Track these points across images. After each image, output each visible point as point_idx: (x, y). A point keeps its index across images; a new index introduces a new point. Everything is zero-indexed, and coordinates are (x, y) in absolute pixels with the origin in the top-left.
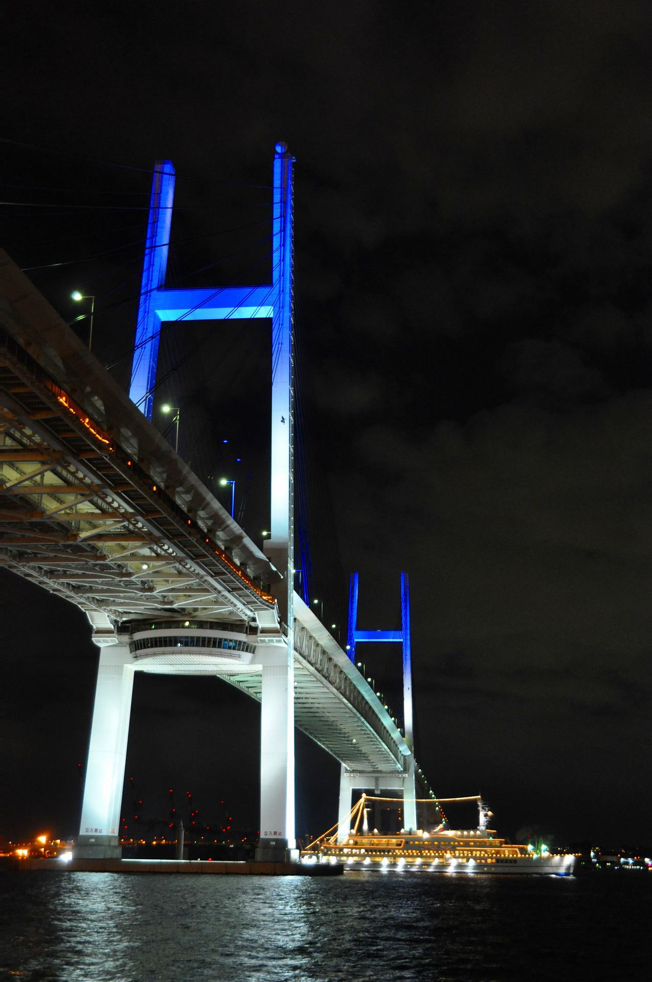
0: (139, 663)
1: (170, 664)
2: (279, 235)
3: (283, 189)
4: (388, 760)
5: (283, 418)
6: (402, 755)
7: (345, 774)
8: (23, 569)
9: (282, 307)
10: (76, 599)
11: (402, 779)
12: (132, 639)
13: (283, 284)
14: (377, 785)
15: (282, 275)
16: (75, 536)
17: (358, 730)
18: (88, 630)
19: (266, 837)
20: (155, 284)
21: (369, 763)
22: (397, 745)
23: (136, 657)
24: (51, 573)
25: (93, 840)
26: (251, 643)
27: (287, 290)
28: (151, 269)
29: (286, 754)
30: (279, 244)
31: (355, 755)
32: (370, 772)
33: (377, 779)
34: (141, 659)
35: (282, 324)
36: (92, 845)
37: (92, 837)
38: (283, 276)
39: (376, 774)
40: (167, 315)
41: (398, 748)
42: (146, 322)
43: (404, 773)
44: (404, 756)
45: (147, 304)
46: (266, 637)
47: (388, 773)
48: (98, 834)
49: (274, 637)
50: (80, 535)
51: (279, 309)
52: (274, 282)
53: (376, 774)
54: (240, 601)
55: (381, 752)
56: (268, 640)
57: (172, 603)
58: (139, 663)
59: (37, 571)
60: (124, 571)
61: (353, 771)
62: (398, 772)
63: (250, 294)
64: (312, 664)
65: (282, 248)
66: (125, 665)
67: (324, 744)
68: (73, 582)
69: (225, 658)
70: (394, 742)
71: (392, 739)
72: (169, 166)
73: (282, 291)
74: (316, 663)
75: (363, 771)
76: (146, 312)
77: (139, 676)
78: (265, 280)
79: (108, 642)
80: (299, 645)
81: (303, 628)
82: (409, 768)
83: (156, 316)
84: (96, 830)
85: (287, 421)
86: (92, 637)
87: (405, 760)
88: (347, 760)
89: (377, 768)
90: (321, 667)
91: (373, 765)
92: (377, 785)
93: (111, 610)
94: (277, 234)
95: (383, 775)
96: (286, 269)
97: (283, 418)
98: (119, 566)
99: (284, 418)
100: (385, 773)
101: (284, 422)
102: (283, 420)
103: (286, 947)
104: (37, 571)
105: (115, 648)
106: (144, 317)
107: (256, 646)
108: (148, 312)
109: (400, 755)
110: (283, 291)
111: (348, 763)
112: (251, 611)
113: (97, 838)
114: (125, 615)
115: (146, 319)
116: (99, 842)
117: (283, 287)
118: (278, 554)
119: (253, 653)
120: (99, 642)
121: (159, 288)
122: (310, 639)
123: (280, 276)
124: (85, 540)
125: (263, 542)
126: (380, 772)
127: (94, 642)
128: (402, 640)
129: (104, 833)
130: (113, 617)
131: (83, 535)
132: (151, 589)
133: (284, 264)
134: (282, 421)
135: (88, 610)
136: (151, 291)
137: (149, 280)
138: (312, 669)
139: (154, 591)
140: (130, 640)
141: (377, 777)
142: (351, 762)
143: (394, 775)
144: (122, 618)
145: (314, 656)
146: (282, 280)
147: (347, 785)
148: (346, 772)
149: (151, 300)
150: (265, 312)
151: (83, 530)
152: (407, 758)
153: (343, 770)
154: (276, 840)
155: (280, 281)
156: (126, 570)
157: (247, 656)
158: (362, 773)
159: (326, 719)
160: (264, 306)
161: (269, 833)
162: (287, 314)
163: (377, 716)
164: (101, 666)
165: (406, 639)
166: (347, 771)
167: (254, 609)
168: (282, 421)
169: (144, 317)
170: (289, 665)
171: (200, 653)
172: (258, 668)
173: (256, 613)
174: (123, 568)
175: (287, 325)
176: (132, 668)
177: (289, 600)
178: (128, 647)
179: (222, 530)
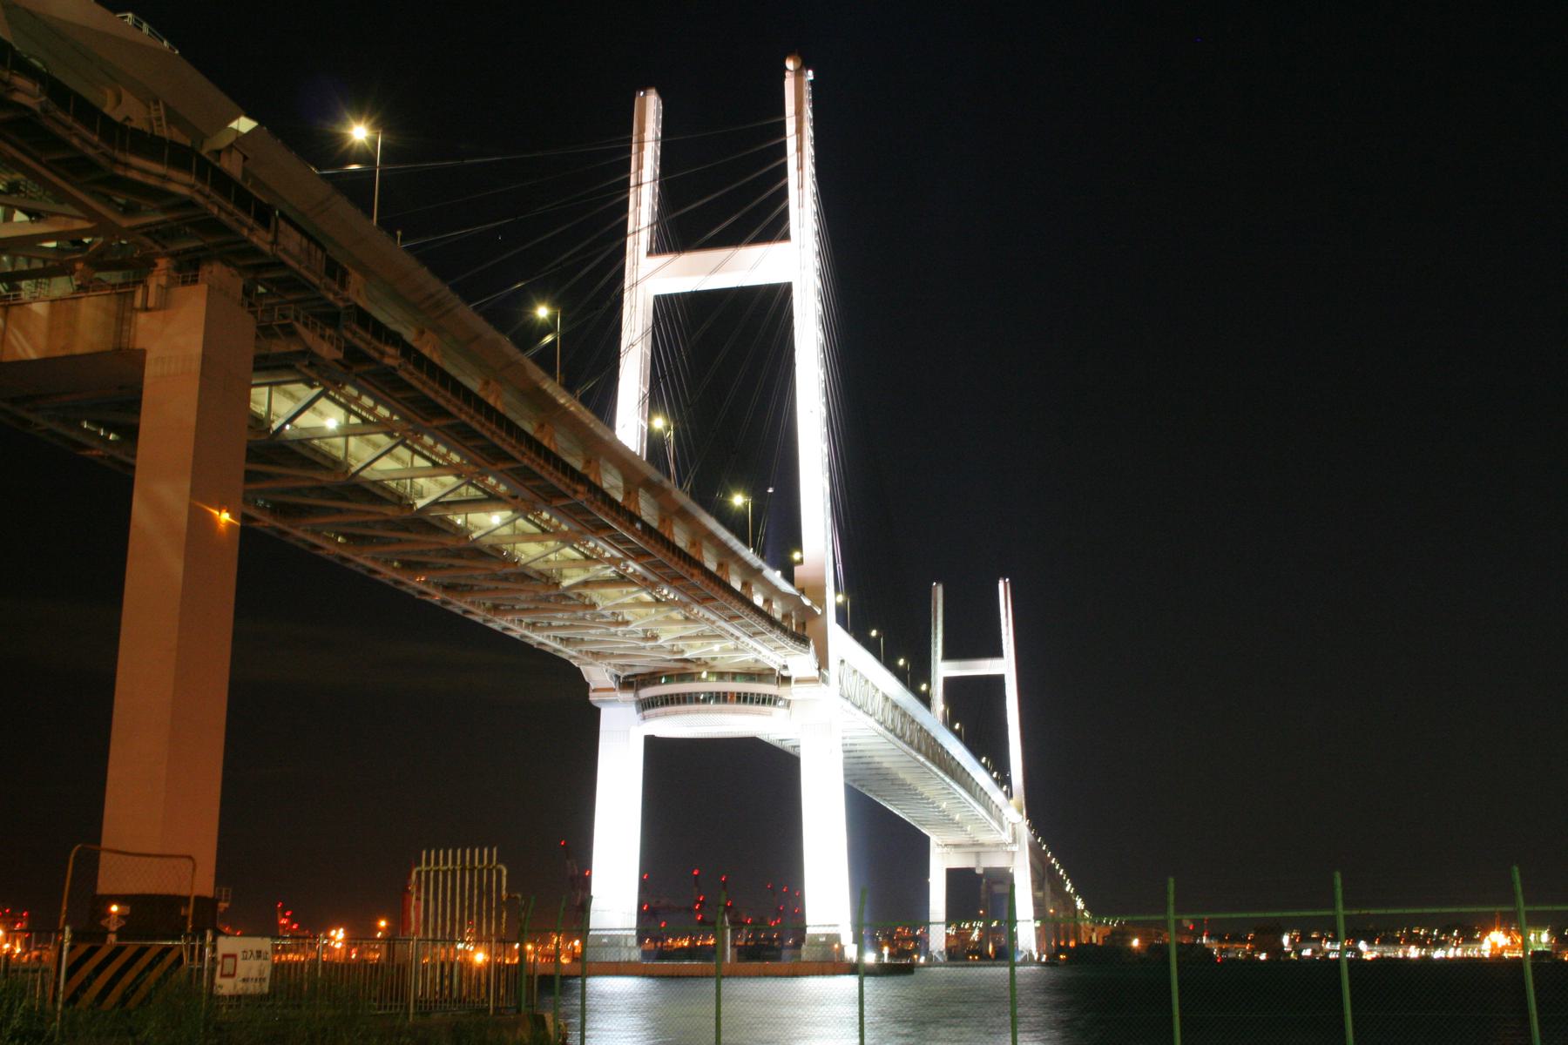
24: (533, 626)
25: (605, 940)
33: (978, 854)
77: (652, 744)
87: (1014, 829)
90: (574, 597)
98: (613, 614)
141: (978, 852)
152: (1017, 826)
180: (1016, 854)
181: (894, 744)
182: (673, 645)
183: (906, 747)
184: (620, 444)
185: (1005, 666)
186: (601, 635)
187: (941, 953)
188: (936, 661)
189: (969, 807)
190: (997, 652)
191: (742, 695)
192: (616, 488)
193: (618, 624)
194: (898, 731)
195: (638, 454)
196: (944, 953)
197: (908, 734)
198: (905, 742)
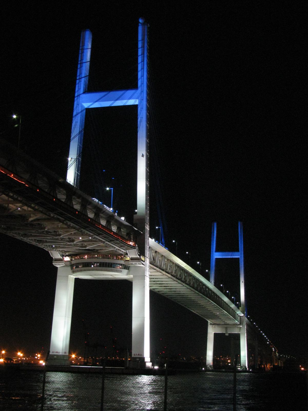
0: (75, 275)
1: (90, 275)
2: (141, 64)
3: (143, 40)
4: (230, 319)
5: (143, 154)
6: (239, 316)
7: (210, 326)
8: (11, 234)
9: (142, 100)
10: (41, 246)
11: (239, 328)
12: (71, 263)
13: (143, 88)
14: (226, 331)
15: (142, 84)
16: (28, 220)
17: (208, 304)
18: (51, 259)
19: (135, 356)
20: (82, 91)
21: (221, 320)
22: (234, 311)
23: (73, 272)
24: (25, 235)
25: (55, 357)
26: (127, 265)
27: (145, 92)
28: (80, 83)
29: (144, 318)
30: (141, 68)
31: (213, 317)
32: (223, 325)
33: (226, 328)
34: (75, 273)
35: (142, 108)
36: (55, 359)
37: (55, 355)
38: (143, 84)
39: (226, 326)
40: (86, 105)
41: (236, 313)
42: (78, 109)
43: (240, 325)
44: (241, 316)
45: (78, 101)
46: (133, 262)
47: (232, 325)
48: (58, 354)
49: (137, 262)
50: (29, 219)
51: (141, 100)
52: (139, 86)
53: (226, 326)
54: (117, 246)
55: (224, 315)
56: (134, 263)
57: (86, 246)
58: (75, 275)
59: (17, 234)
60: (58, 233)
61: (214, 324)
62: (237, 325)
63: (124, 93)
64: (169, 273)
65: (142, 70)
66: (69, 276)
67: (194, 311)
68: (38, 238)
69: (114, 272)
70: (233, 309)
71: (231, 308)
72: (88, 32)
73: (142, 92)
74: (172, 272)
75: (220, 324)
76: (78, 104)
77: (77, 281)
78: (134, 86)
79: (60, 265)
80: (159, 264)
81: (162, 256)
82: (243, 322)
83: (82, 106)
84: (57, 352)
85: (145, 156)
86: (52, 263)
87: (240, 318)
88: (210, 319)
89: (226, 323)
90: (176, 274)
91: (223, 321)
92: (226, 331)
93: (60, 250)
94: (140, 63)
95: (229, 326)
96: (144, 80)
97: (143, 154)
98: (55, 231)
99: (144, 154)
100: (231, 325)
101: (143, 157)
102: (143, 156)
103: (54, 407)
104: (17, 234)
105: (63, 268)
106: (77, 107)
107: (129, 266)
108: (79, 104)
109: (237, 316)
110: (143, 92)
111: (210, 320)
112: (124, 250)
113: (57, 356)
114: (67, 252)
115: (78, 108)
116: (58, 357)
117: (143, 89)
118: (142, 221)
119: (128, 269)
120: (56, 265)
121: (84, 93)
122: (167, 261)
123: (141, 84)
124: (32, 221)
125: (133, 216)
126: (228, 324)
127: (54, 265)
128: (239, 257)
129: (61, 354)
130: (61, 253)
131: (31, 219)
132: (73, 241)
133: (143, 78)
134: (142, 156)
135: (49, 250)
136: (80, 95)
137: (79, 89)
138: (169, 275)
139: (74, 242)
140: (70, 264)
141: (226, 327)
142: (212, 319)
143: (235, 326)
144: (66, 254)
145: (170, 269)
146: (142, 86)
147: (211, 332)
148: (210, 325)
149: (80, 99)
150: (131, 102)
151: (30, 217)
152: (242, 318)
153: (209, 324)
154: (139, 358)
155: (141, 86)
156: (59, 233)
157: (126, 271)
158: (218, 325)
159: (190, 299)
160: (131, 99)
161: (136, 355)
162: (145, 103)
163: (219, 297)
164: (58, 276)
165: (241, 257)
166: (211, 324)
167: (126, 249)
168: (142, 156)
169: (77, 107)
170: (146, 275)
171: (102, 270)
172: (132, 276)
173: (127, 251)
174: (57, 232)
175: (145, 108)
176: (72, 277)
177: (146, 244)
178: (70, 266)
179: (102, 213)
180: (241, 328)
181: (172, 278)
182: (83, 244)
183: (188, 286)
184: (68, 182)
185: (238, 255)
186: (50, 239)
187: (210, 366)
188: (213, 252)
189: (221, 311)
190: (237, 250)
191: (110, 264)
192: (89, 215)
193: (57, 235)
194: (183, 279)
195: (73, 185)
196: (212, 366)
197: (188, 280)
198: (186, 284)
